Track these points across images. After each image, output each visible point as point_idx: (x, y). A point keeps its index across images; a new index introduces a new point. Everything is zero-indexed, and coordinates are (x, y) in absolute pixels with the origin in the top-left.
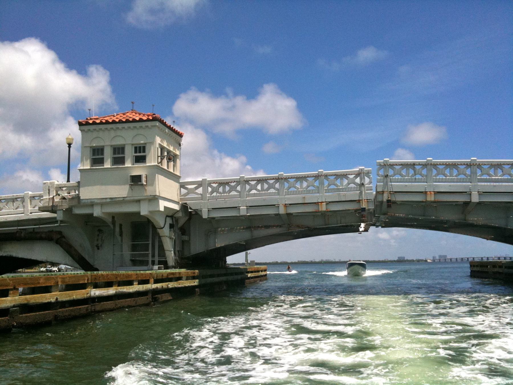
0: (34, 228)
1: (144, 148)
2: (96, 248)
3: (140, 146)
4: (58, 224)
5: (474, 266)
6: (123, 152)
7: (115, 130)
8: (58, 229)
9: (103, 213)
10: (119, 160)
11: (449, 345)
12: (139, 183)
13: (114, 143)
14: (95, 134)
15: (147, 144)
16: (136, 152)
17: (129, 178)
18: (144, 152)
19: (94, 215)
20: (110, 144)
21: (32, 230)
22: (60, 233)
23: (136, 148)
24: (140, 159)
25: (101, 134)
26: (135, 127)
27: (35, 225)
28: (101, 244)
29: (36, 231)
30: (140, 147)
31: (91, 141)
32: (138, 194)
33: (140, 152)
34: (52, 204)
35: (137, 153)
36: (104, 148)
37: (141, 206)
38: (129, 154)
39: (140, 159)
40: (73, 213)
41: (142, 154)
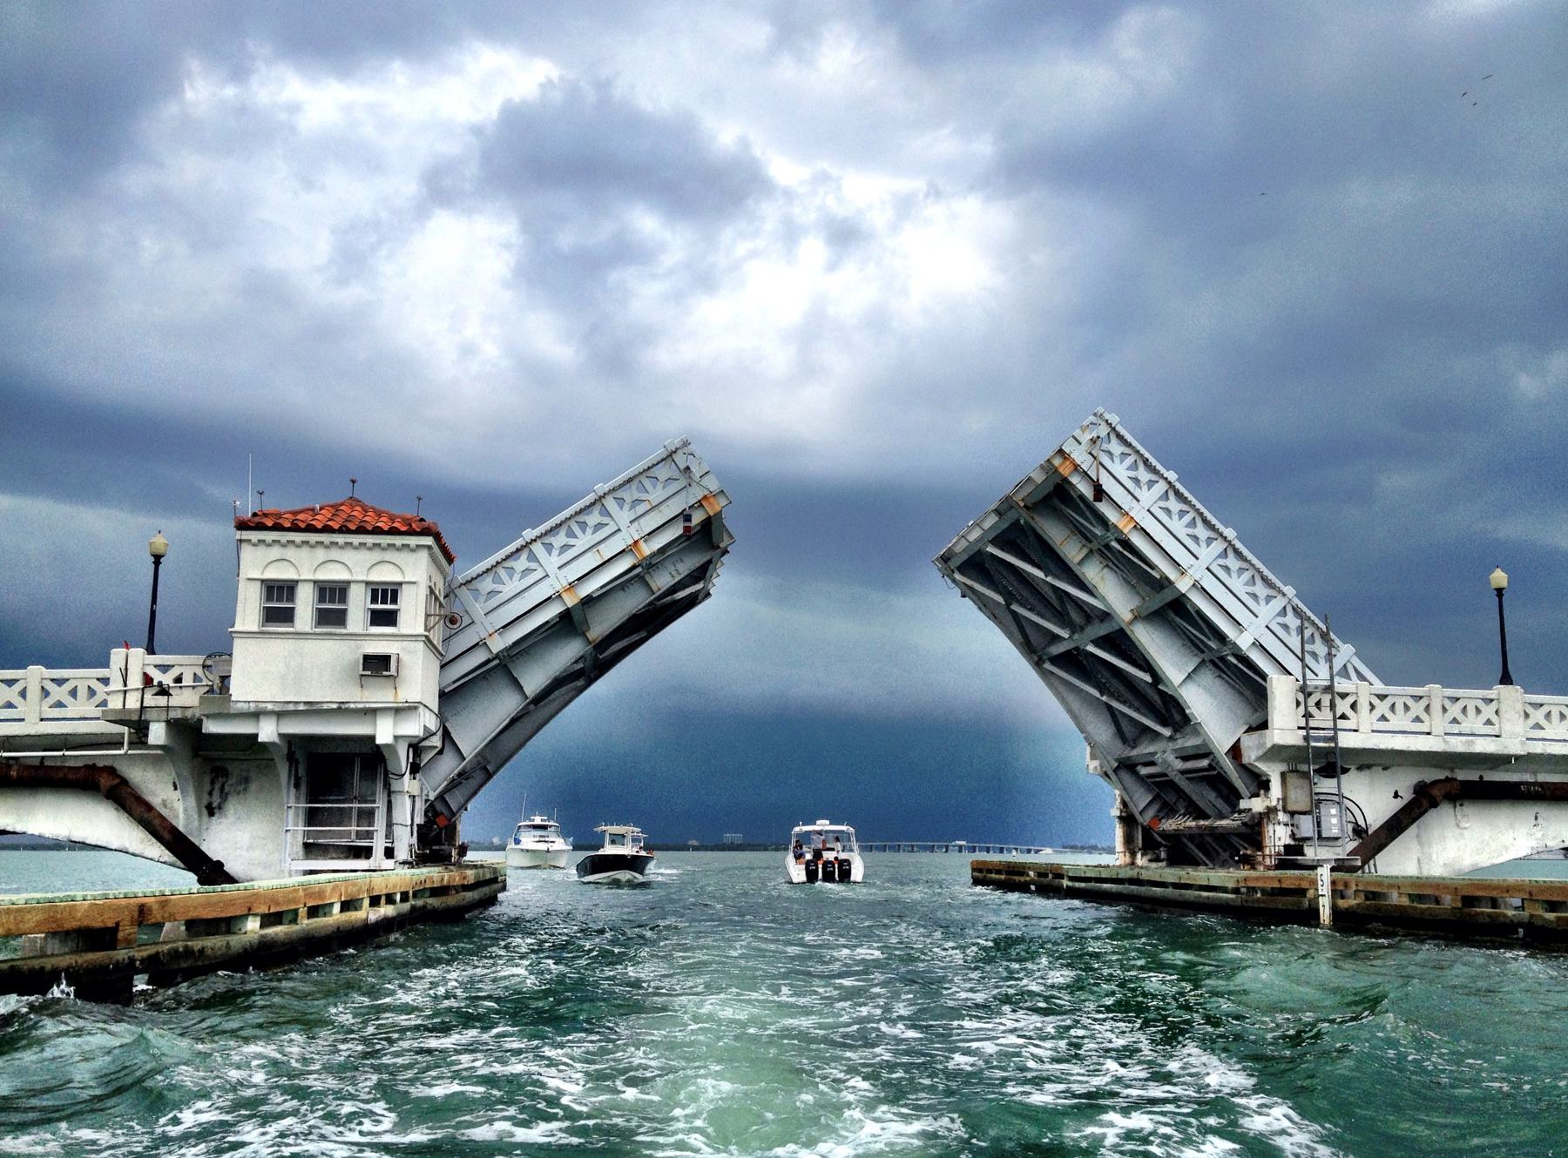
0: (43, 757)
1: (395, 595)
2: (205, 812)
3: (384, 587)
4: (122, 752)
5: (980, 871)
6: (291, 598)
7: (327, 547)
8: (107, 763)
9: (280, 735)
10: (331, 616)
11: (1324, 1128)
12: (385, 673)
13: (321, 576)
14: (276, 552)
15: (404, 586)
16: (374, 600)
17: (361, 661)
18: (394, 601)
19: (260, 740)
20: (364, 578)
21: (37, 763)
22: (111, 771)
23: (375, 592)
24: (385, 618)
25: (290, 553)
26: (363, 545)
27: (45, 750)
28: (220, 804)
29: (47, 763)
30: (385, 592)
31: (369, 569)
32: (378, 695)
33: (384, 602)
34: (138, 705)
35: (272, 601)
36: (349, 586)
37: (378, 722)
38: (358, 606)
39: (385, 618)
40: (203, 731)
41: (389, 607)
